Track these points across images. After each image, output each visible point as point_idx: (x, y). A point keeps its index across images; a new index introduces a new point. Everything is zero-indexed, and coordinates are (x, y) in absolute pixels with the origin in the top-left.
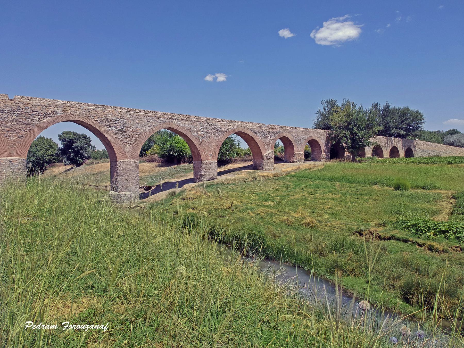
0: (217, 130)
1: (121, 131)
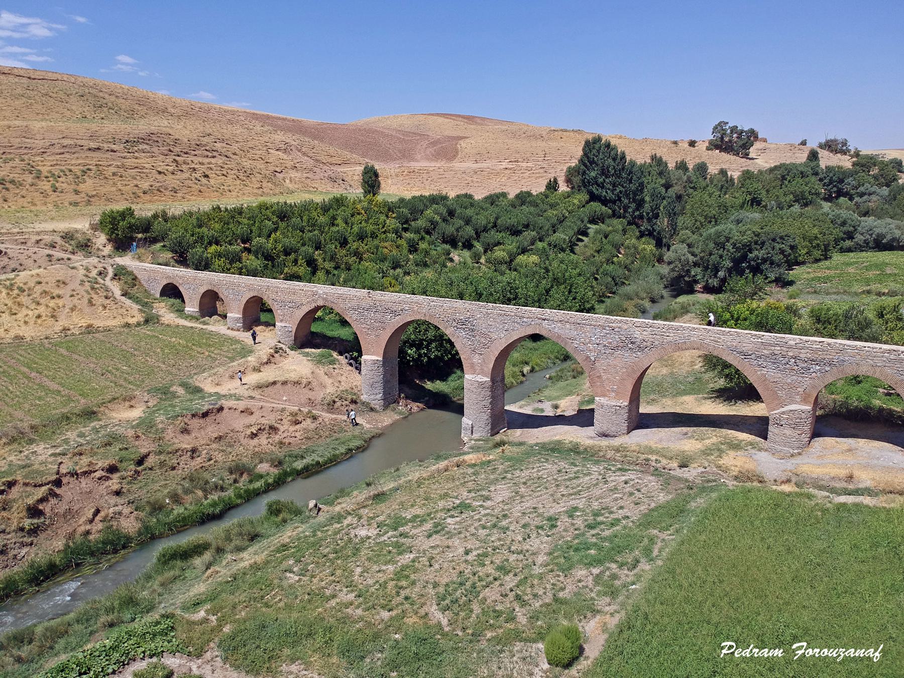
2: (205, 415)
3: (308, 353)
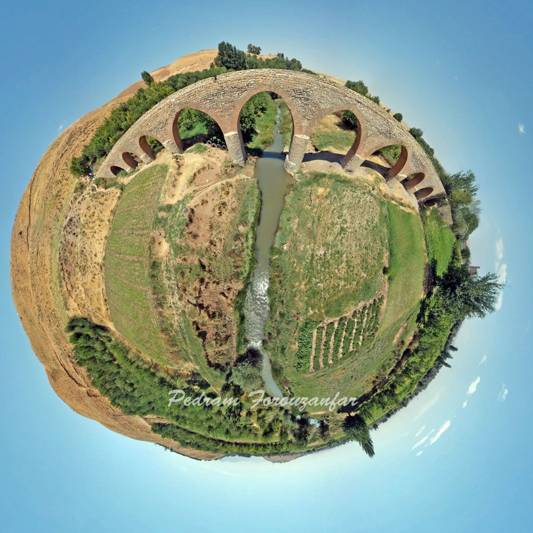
0: (390, 133)
1: (304, 104)
2: (191, 220)
3: (190, 150)
